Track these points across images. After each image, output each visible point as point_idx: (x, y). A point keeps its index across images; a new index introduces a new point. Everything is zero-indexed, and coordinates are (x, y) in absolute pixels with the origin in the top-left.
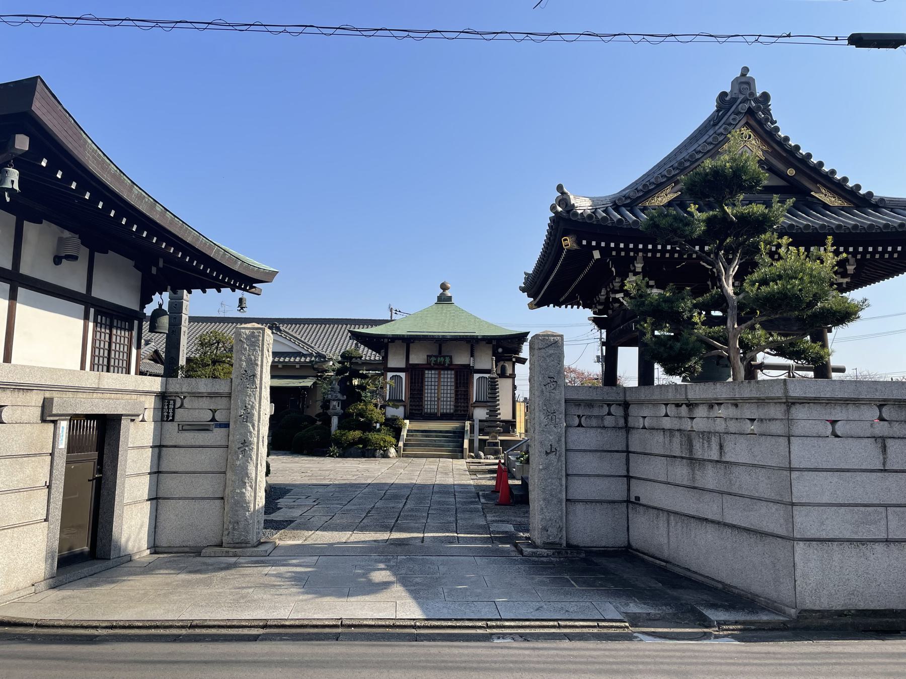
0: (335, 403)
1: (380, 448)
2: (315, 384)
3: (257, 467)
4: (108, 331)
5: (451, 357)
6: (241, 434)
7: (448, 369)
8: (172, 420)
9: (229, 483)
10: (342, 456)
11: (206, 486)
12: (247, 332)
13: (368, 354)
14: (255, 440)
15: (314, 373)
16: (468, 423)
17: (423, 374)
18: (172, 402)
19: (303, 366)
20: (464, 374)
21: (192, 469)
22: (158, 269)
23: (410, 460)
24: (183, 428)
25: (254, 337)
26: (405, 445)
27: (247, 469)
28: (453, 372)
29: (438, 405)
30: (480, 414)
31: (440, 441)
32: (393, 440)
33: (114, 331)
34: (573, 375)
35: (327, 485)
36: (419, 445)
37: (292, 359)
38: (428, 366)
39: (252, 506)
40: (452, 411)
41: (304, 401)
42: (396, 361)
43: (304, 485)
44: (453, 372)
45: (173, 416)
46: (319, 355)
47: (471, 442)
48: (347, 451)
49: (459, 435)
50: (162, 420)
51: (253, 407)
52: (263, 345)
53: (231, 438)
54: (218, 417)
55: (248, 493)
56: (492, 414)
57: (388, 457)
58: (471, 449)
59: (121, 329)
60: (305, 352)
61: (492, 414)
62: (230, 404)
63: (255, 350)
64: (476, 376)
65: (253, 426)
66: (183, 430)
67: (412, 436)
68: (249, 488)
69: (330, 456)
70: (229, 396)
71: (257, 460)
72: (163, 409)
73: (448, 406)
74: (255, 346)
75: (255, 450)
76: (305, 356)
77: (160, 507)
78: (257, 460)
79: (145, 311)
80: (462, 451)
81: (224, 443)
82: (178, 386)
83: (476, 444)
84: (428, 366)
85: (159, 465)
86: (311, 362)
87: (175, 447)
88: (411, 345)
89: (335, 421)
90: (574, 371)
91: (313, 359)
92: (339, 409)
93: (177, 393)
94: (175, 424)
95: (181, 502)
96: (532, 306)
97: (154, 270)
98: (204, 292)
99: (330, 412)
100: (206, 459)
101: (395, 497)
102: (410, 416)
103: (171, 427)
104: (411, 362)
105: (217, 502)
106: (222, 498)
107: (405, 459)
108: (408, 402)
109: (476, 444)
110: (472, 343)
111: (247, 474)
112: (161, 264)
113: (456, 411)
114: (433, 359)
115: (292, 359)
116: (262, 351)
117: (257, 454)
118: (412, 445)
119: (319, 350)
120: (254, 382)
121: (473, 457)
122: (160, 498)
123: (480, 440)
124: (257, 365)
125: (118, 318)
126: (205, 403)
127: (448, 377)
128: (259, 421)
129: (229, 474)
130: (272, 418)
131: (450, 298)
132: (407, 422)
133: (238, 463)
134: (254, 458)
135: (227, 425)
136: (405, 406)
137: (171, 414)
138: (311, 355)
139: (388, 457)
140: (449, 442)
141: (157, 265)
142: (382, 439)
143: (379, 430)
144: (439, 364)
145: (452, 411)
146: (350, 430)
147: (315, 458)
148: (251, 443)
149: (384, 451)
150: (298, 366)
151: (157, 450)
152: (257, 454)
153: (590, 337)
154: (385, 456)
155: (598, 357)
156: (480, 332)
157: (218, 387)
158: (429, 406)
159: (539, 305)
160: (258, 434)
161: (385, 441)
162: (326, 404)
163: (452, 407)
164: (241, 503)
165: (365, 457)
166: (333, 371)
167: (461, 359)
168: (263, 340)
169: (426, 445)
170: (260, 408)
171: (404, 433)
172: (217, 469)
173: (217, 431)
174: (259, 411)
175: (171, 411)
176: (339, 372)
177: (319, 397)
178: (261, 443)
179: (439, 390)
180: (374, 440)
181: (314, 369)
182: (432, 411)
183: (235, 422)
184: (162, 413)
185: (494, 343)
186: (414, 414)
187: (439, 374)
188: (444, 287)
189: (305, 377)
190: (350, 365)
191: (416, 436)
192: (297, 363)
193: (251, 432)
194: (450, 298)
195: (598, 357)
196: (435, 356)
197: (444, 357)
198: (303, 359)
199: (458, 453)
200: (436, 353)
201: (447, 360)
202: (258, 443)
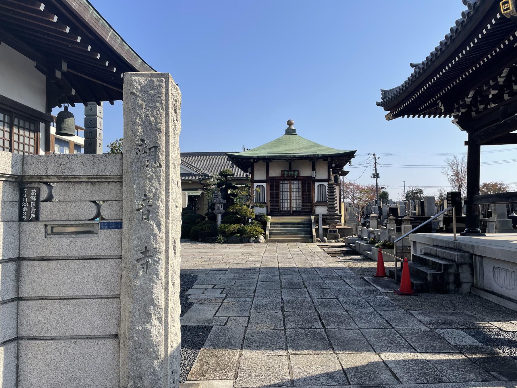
0: (219, 205)
1: (253, 236)
2: (202, 193)
3: (167, 288)
4: (8, 130)
5: (298, 171)
6: (139, 238)
8: (37, 219)
9: (125, 315)
10: (226, 242)
11: (92, 318)
12: (142, 80)
13: (238, 172)
14: (163, 246)
15: (201, 186)
16: (313, 217)
17: (279, 184)
18: (34, 192)
19: (194, 182)
20: (307, 184)
21: (70, 293)
22: (63, 73)
23: (276, 244)
24: (52, 231)
25: (153, 88)
26: (270, 233)
27: (152, 292)
28: (300, 182)
29: (290, 205)
30: (321, 211)
31: (295, 230)
32: (262, 231)
33: (16, 130)
34: (352, 187)
35: (226, 270)
36: (280, 233)
38: (283, 178)
39: (162, 349)
40: (300, 209)
41: (195, 205)
42: (260, 175)
43: (206, 270)
44: (300, 182)
45: (37, 213)
46: (204, 175)
47: (317, 230)
48: (230, 238)
49: (308, 226)
50: (21, 219)
51: (156, 196)
52: (167, 100)
53: (125, 244)
54: (107, 213)
55: (156, 330)
57: (259, 242)
58: (318, 235)
59: (24, 129)
60: (195, 173)
62: (122, 193)
63: (155, 107)
64: (317, 184)
65: (159, 225)
66: (53, 233)
67: (274, 227)
68: (156, 322)
69: (219, 243)
70: (120, 180)
71: (167, 277)
72: (21, 201)
74: (155, 101)
75: (163, 262)
76: (195, 175)
77: (22, 353)
78: (167, 277)
79: (52, 113)
81: (115, 252)
82: (41, 167)
83: (321, 232)
84: (283, 178)
85: (18, 288)
86: (199, 179)
87: (42, 259)
88: (270, 164)
89: (219, 218)
90: (353, 185)
91: (200, 177)
92: (221, 209)
93: (40, 177)
94: (40, 225)
95: (54, 344)
96: (389, 118)
97: (58, 74)
98: (112, 103)
99: (215, 211)
100: (92, 277)
101: (292, 285)
102: (271, 213)
103: (34, 231)
104: (270, 175)
105: (109, 343)
106: (117, 336)
107: (272, 243)
108: (269, 203)
109: (321, 232)
110: (313, 160)
111: (152, 300)
112: (65, 67)
113: (303, 209)
114: (286, 173)
116: (167, 109)
117: (167, 269)
118: (275, 234)
119: (204, 171)
120: (156, 158)
121: (319, 241)
122: (22, 338)
123: (323, 229)
124: (160, 131)
125: (20, 117)
126: (85, 192)
128: (167, 217)
129: (124, 300)
130: (185, 212)
131: (294, 131)
132: (269, 217)
133: (138, 283)
134: (162, 274)
135: (118, 225)
136: (267, 207)
137: (33, 210)
139: (259, 242)
140: (301, 230)
141: (60, 68)
142: (254, 230)
143: (252, 223)
144: (290, 177)
145: (300, 209)
146: (231, 224)
147: (207, 244)
148: (156, 252)
149: (256, 238)
150: (190, 182)
151: (12, 266)
152: (167, 269)
153: (368, 162)
154: (257, 241)
155: (373, 174)
156: (320, 152)
157: (102, 166)
158: (286, 206)
159: (396, 116)
160: (167, 237)
161: (256, 231)
162: (212, 207)
163: (300, 206)
164: (144, 346)
165: (242, 243)
166: (215, 185)
167: (306, 172)
168: (167, 93)
170: (167, 197)
171: (268, 225)
172: (107, 292)
173: (105, 233)
174: (167, 202)
175: (33, 205)
176: (219, 185)
177: (206, 202)
178: (171, 251)
179: (291, 196)
180: (248, 231)
181: (202, 184)
183: (131, 220)
184: (21, 208)
185: (329, 159)
186: (275, 211)
187: (290, 184)
188: (290, 123)
189: (196, 190)
190: (225, 182)
191: (277, 227)
192: (190, 180)
193: (155, 235)
194: (294, 131)
195: (373, 174)
196: (288, 171)
197: (294, 171)
198: (194, 178)
199: (309, 238)
200: (288, 169)
201: (296, 173)
202: (167, 251)
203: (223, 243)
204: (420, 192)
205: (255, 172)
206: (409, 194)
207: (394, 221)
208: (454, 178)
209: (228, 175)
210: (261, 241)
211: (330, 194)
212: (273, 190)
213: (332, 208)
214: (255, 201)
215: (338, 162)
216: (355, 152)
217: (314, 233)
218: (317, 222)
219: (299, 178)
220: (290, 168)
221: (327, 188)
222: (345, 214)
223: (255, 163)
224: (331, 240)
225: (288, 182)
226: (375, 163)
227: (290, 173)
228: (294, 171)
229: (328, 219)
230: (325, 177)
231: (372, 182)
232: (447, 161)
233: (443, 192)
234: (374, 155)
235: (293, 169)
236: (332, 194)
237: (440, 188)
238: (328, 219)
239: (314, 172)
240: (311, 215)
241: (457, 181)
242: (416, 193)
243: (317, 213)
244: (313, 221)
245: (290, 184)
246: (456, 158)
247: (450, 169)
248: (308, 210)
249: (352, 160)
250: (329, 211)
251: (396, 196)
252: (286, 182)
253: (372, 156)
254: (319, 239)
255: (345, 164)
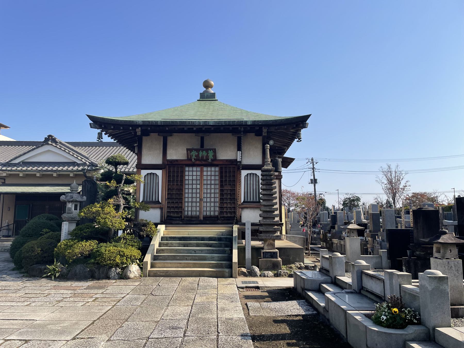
1: (117, 265)
5: (214, 151)
7: (211, 165)
16: (235, 228)
17: (183, 172)
20: (229, 171)
26: (155, 258)
28: (217, 169)
29: (200, 207)
30: (250, 216)
31: (202, 251)
32: (136, 253)
36: (174, 258)
37: (65, 168)
38: (189, 163)
40: (217, 214)
42: (152, 156)
44: (217, 169)
46: (92, 164)
47: (242, 251)
49: (226, 242)
56: (268, 215)
58: (241, 263)
60: (79, 162)
61: (268, 215)
64: (244, 173)
67: (167, 245)
69: (49, 277)
73: (211, 207)
76: (79, 165)
80: (230, 266)
83: (248, 254)
84: (189, 163)
86: (83, 170)
88: (169, 139)
90: (289, 192)
91: (86, 167)
102: (167, 220)
104: (169, 158)
108: (165, 204)
109: (248, 254)
110: (239, 131)
113: (221, 213)
114: (194, 153)
115: (65, 168)
118: (165, 258)
127: (211, 174)
131: (213, 95)
132: (162, 228)
136: (161, 209)
138: (84, 164)
145: (217, 214)
149: (123, 269)
154: (123, 276)
155: (311, 180)
158: (190, 208)
163: (217, 209)
167: (227, 153)
169: (183, 258)
171: (156, 243)
179: (201, 188)
180: (107, 255)
182: (194, 213)
187: (202, 171)
188: (207, 85)
191: (172, 245)
194: (213, 95)
195: (311, 180)
196: (197, 150)
197: (207, 150)
199: (225, 270)
200: (198, 147)
201: (211, 154)
203: (57, 279)
204: (357, 199)
205: (145, 152)
206: (346, 201)
207: (455, 251)
208: (389, 186)
209: (120, 163)
210: (132, 276)
211: (264, 187)
212: (173, 180)
213: (268, 213)
214: (141, 200)
215: (281, 134)
216: (308, 117)
217: (235, 259)
218: (242, 235)
219: (215, 163)
220: (202, 145)
221: (260, 177)
222: (286, 222)
223: (144, 138)
224: (266, 272)
225: (199, 169)
226: (313, 168)
227: (201, 153)
228: (207, 150)
229: (261, 232)
230: (258, 161)
231: (310, 189)
232: (381, 169)
233: (379, 200)
234: (312, 160)
235: (206, 147)
236: (268, 187)
237: (375, 196)
238: (261, 232)
239: (239, 153)
240: (232, 224)
241: (392, 190)
242: (353, 200)
243: (243, 221)
244: (235, 234)
245: (202, 171)
246: (389, 167)
247: (385, 177)
248: (229, 215)
249: (303, 132)
250: (264, 218)
251: (333, 202)
252: (195, 169)
253: (310, 161)
254: (244, 270)
255: (288, 145)
